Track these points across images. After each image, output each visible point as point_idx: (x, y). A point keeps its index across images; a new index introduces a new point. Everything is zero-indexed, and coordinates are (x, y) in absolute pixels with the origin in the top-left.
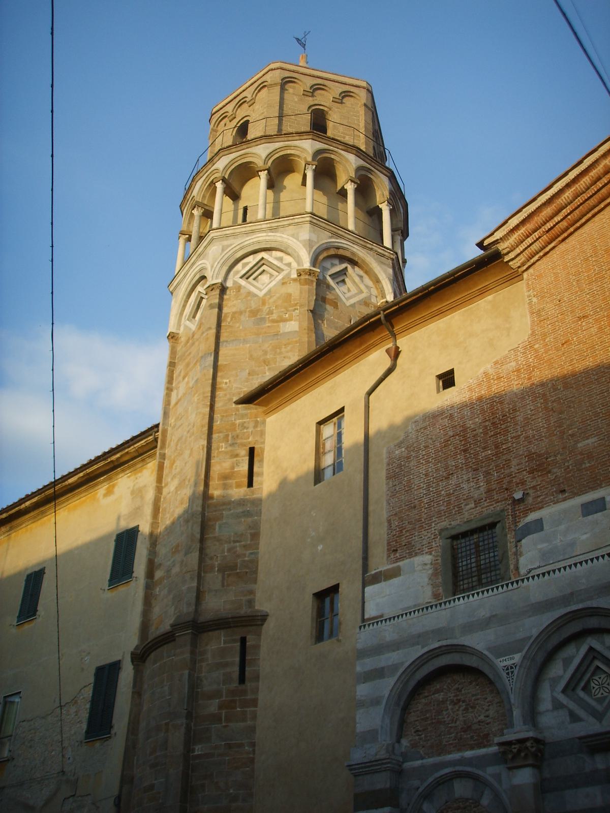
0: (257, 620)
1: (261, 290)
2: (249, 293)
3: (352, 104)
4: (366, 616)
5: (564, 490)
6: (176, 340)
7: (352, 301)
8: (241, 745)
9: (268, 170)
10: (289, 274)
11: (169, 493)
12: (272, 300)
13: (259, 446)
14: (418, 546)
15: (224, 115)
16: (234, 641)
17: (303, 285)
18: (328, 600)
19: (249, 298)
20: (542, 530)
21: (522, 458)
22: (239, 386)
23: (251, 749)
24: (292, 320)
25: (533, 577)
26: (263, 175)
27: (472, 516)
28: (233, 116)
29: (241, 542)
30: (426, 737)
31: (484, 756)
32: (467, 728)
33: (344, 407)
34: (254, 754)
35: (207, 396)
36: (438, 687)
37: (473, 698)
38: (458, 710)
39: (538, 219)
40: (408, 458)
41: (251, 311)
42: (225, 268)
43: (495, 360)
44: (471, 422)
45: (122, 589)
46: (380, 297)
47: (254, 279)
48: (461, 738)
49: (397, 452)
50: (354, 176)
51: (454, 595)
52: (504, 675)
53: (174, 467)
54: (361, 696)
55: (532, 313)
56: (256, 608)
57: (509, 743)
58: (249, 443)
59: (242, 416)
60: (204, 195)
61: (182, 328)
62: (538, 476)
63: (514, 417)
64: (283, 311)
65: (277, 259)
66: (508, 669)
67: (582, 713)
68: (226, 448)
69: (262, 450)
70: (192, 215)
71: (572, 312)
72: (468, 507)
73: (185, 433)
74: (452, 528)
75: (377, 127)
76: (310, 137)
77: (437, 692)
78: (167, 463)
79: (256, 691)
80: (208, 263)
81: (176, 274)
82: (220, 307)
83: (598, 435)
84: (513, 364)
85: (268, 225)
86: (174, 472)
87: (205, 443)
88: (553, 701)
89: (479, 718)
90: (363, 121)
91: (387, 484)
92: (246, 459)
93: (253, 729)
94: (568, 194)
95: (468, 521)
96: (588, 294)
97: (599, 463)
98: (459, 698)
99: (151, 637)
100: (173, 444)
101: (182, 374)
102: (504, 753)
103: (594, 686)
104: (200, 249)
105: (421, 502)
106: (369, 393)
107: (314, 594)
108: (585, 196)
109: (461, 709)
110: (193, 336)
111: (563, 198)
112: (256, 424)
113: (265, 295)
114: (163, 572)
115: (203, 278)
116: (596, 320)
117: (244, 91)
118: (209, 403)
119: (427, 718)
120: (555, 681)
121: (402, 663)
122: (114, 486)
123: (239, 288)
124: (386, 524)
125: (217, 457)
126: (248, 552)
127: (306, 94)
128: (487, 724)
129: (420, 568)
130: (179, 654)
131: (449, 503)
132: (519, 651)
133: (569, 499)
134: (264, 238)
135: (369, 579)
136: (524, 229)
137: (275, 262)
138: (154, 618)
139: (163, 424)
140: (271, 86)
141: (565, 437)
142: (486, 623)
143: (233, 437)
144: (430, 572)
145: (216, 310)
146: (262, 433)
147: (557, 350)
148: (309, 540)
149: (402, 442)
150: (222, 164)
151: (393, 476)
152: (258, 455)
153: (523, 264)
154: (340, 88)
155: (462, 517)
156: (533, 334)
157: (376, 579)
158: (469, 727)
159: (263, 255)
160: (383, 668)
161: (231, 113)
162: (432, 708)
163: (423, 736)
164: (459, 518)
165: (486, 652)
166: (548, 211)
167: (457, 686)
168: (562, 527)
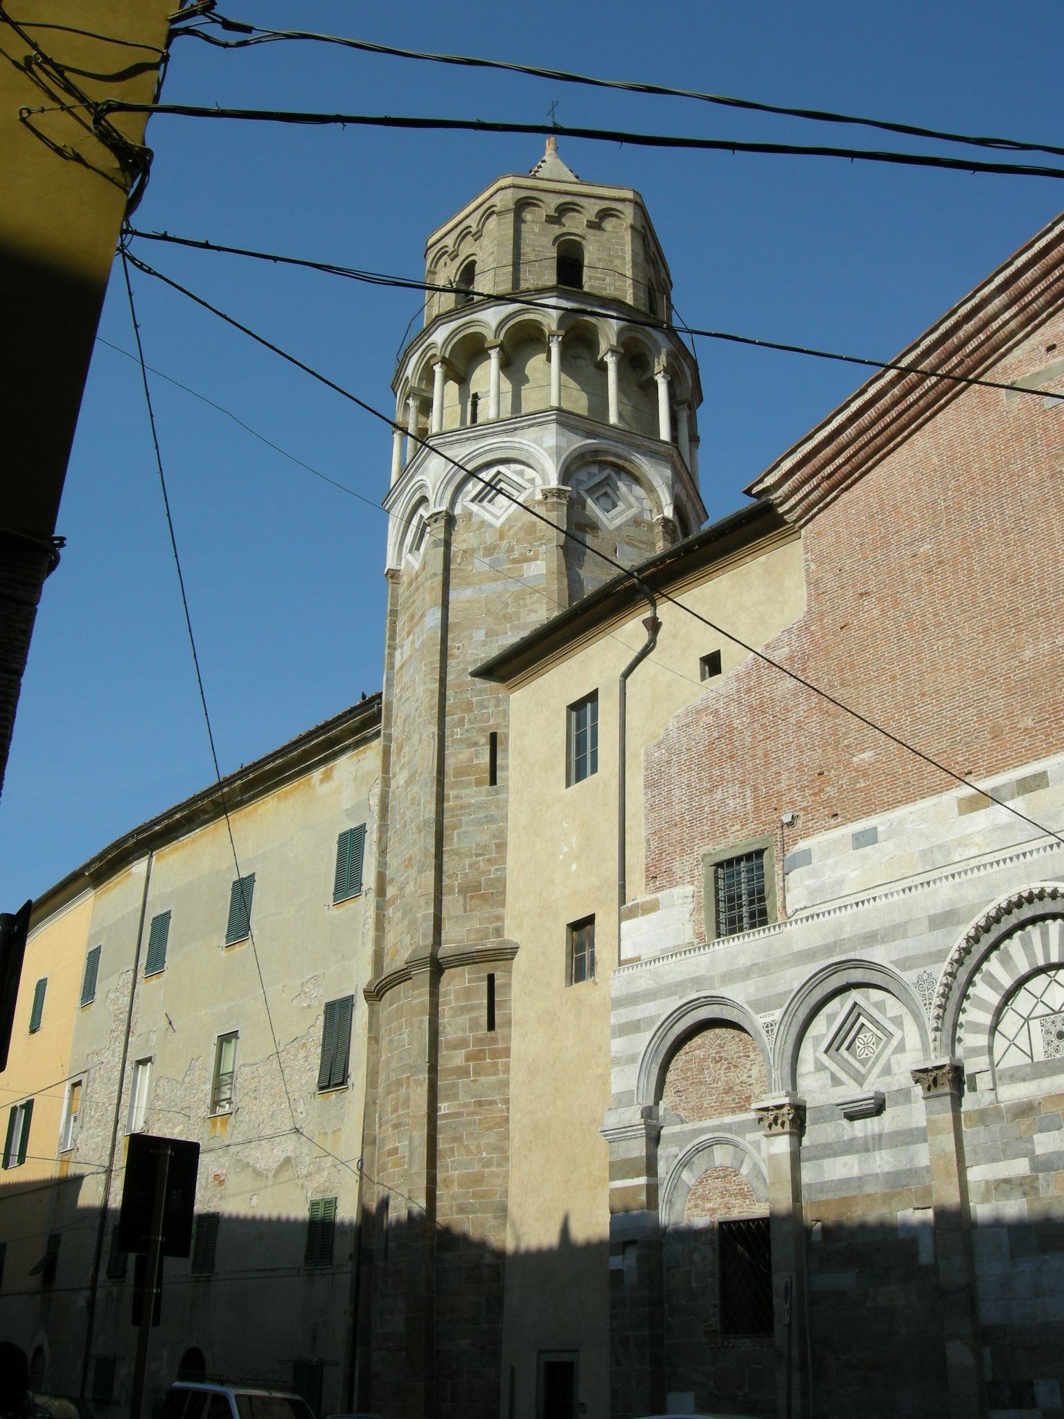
0: (506, 954)
1: (498, 518)
2: (483, 523)
3: (614, 227)
4: (623, 958)
5: (837, 815)
6: (397, 579)
7: (617, 522)
8: (493, 1103)
9: (501, 346)
10: (533, 493)
11: (398, 787)
12: (512, 532)
14: (680, 874)
15: (443, 251)
16: (481, 979)
17: (550, 511)
19: (483, 529)
20: (810, 863)
21: (792, 772)
22: (475, 651)
24: (537, 559)
25: (796, 921)
26: (494, 354)
27: (738, 840)
28: (455, 253)
30: (686, 1098)
31: (743, 1122)
32: (730, 1089)
33: (596, 691)
34: (508, 1112)
35: (436, 668)
36: (700, 1042)
37: (736, 1056)
38: (720, 1069)
40: (669, 762)
41: (486, 548)
42: (451, 490)
43: (766, 643)
44: (738, 721)
45: (350, 905)
46: (655, 511)
47: (490, 501)
48: (722, 1101)
49: (656, 754)
50: (615, 344)
53: (402, 753)
54: (617, 1052)
55: (809, 584)
56: (506, 937)
57: (766, 1109)
58: (490, 727)
59: (481, 692)
61: (403, 563)
62: (810, 795)
64: (526, 547)
65: (516, 472)
66: (767, 1027)
67: (843, 1076)
68: (462, 734)
69: (507, 736)
70: (407, 405)
71: (854, 586)
72: (733, 829)
73: (413, 711)
74: (716, 854)
75: (653, 249)
76: (555, 294)
78: (394, 746)
79: (508, 1038)
80: (427, 480)
81: (392, 486)
82: (447, 544)
83: (874, 749)
84: (787, 649)
86: (402, 761)
87: (435, 729)
88: (815, 1062)
89: (742, 1079)
90: (630, 253)
91: (646, 794)
92: (487, 749)
93: (506, 1084)
94: (851, 431)
95: (732, 847)
96: (871, 564)
97: (875, 783)
98: (721, 1055)
99: (387, 972)
100: (400, 721)
101: (406, 629)
103: (860, 1045)
105: (682, 818)
107: (569, 925)
108: (871, 433)
110: (417, 578)
112: (498, 701)
113: (504, 524)
114: (396, 889)
115: (424, 500)
116: (879, 599)
117: (467, 217)
118: (438, 677)
120: (817, 1040)
121: (659, 1016)
122: (331, 770)
123: (470, 515)
125: (452, 746)
126: (493, 869)
127: (551, 220)
128: (750, 1085)
129: (680, 901)
130: (415, 994)
131: (713, 823)
132: (780, 1006)
133: (842, 825)
135: (626, 911)
140: (499, 214)
142: (746, 973)
143: (469, 720)
144: (691, 906)
145: (441, 549)
146: (505, 714)
147: (835, 634)
150: (439, 336)
151: (651, 784)
152: (502, 743)
153: (800, 518)
154: (596, 204)
156: (809, 612)
157: (632, 913)
158: (731, 1088)
159: (501, 468)
160: (639, 1021)
161: (450, 249)
163: (684, 1097)
165: (746, 1007)
167: (719, 1041)
168: (831, 861)
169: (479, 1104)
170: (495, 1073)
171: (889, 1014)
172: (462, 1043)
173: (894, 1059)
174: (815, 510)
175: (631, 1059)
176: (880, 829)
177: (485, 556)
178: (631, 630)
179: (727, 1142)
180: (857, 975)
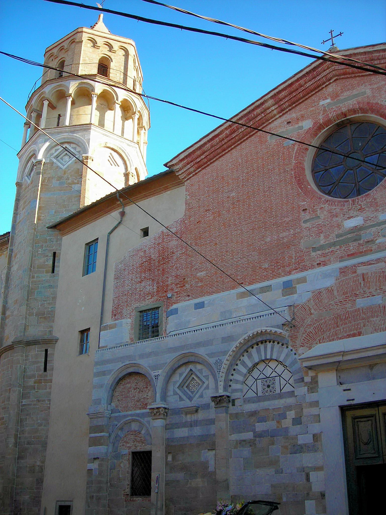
0: (52, 341)
2: (58, 167)
5: (189, 295)
12: (69, 172)
13: (58, 252)
16: (42, 351)
18: (86, 334)
21: (173, 277)
23: (49, 403)
29: (47, 301)
33: (98, 238)
34: (50, 405)
39: (194, 156)
51: (139, 340)
52: (154, 379)
55: (186, 204)
56: (53, 335)
58: (53, 250)
60: (37, 105)
63: (172, 256)
65: (73, 148)
66: (156, 376)
67: (184, 397)
69: (60, 254)
74: (140, 307)
77: (129, 383)
79: (52, 375)
85: (70, 129)
88: (173, 391)
93: (50, 393)
94: (208, 145)
98: (137, 386)
100: (16, 245)
102: (151, 413)
103: (191, 386)
104: (34, 139)
106: (110, 233)
109: (137, 392)
111: (205, 147)
113: (66, 168)
119: (123, 395)
120: (175, 382)
124: (112, 302)
134: (67, 136)
136: (186, 160)
137: (72, 150)
138: (5, 335)
139: (12, 233)
141: (193, 270)
142: (149, 355)
146: (60, 245)
148: (78, 304)
149: (122, 261)
151: (117, 278)
153: (185, 177)
155: (145, 302)
157: (106, 328)
162: (125, 390)
163: (121, 402)
164: (144, 303)
166: (198, 153)
167: (136, 381)
169: (39, 401)
170: (46, 389)
171: (204, 375)
172: (33, 376)
173: (178, 396)
174: (191, 175)
175: (102, 386)
176: (205, 302)
177: (57, 180)
178: (115, 214)
179: (137, 421)
180: (192, 359)
